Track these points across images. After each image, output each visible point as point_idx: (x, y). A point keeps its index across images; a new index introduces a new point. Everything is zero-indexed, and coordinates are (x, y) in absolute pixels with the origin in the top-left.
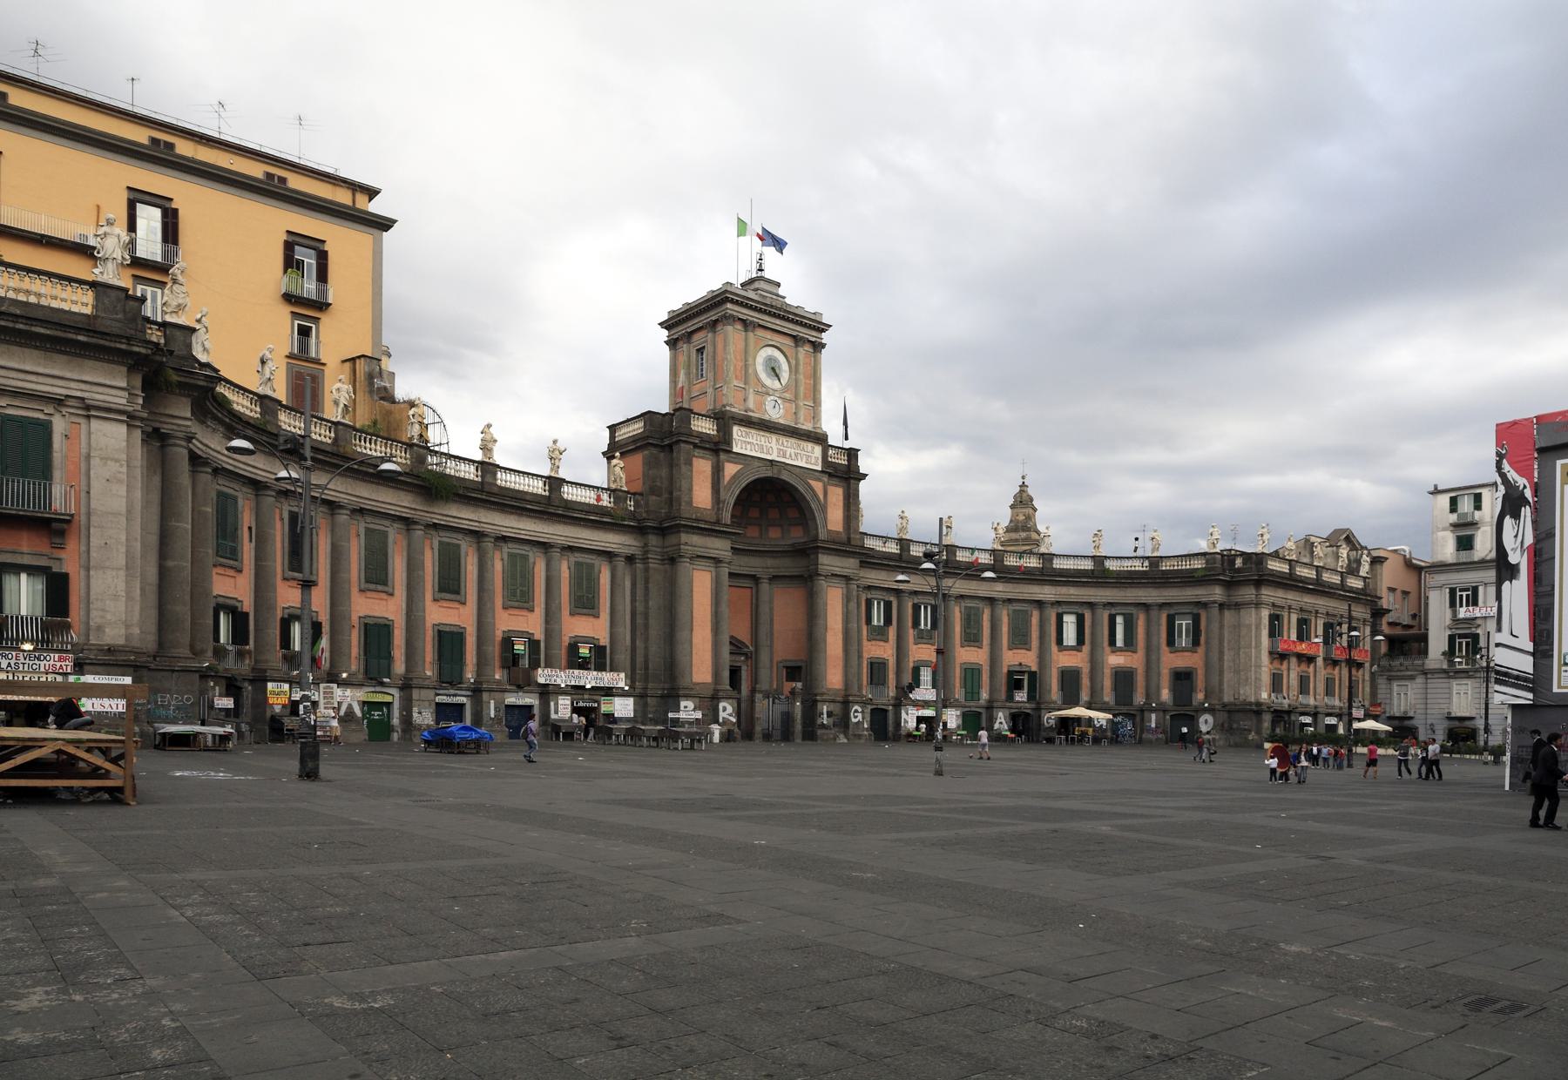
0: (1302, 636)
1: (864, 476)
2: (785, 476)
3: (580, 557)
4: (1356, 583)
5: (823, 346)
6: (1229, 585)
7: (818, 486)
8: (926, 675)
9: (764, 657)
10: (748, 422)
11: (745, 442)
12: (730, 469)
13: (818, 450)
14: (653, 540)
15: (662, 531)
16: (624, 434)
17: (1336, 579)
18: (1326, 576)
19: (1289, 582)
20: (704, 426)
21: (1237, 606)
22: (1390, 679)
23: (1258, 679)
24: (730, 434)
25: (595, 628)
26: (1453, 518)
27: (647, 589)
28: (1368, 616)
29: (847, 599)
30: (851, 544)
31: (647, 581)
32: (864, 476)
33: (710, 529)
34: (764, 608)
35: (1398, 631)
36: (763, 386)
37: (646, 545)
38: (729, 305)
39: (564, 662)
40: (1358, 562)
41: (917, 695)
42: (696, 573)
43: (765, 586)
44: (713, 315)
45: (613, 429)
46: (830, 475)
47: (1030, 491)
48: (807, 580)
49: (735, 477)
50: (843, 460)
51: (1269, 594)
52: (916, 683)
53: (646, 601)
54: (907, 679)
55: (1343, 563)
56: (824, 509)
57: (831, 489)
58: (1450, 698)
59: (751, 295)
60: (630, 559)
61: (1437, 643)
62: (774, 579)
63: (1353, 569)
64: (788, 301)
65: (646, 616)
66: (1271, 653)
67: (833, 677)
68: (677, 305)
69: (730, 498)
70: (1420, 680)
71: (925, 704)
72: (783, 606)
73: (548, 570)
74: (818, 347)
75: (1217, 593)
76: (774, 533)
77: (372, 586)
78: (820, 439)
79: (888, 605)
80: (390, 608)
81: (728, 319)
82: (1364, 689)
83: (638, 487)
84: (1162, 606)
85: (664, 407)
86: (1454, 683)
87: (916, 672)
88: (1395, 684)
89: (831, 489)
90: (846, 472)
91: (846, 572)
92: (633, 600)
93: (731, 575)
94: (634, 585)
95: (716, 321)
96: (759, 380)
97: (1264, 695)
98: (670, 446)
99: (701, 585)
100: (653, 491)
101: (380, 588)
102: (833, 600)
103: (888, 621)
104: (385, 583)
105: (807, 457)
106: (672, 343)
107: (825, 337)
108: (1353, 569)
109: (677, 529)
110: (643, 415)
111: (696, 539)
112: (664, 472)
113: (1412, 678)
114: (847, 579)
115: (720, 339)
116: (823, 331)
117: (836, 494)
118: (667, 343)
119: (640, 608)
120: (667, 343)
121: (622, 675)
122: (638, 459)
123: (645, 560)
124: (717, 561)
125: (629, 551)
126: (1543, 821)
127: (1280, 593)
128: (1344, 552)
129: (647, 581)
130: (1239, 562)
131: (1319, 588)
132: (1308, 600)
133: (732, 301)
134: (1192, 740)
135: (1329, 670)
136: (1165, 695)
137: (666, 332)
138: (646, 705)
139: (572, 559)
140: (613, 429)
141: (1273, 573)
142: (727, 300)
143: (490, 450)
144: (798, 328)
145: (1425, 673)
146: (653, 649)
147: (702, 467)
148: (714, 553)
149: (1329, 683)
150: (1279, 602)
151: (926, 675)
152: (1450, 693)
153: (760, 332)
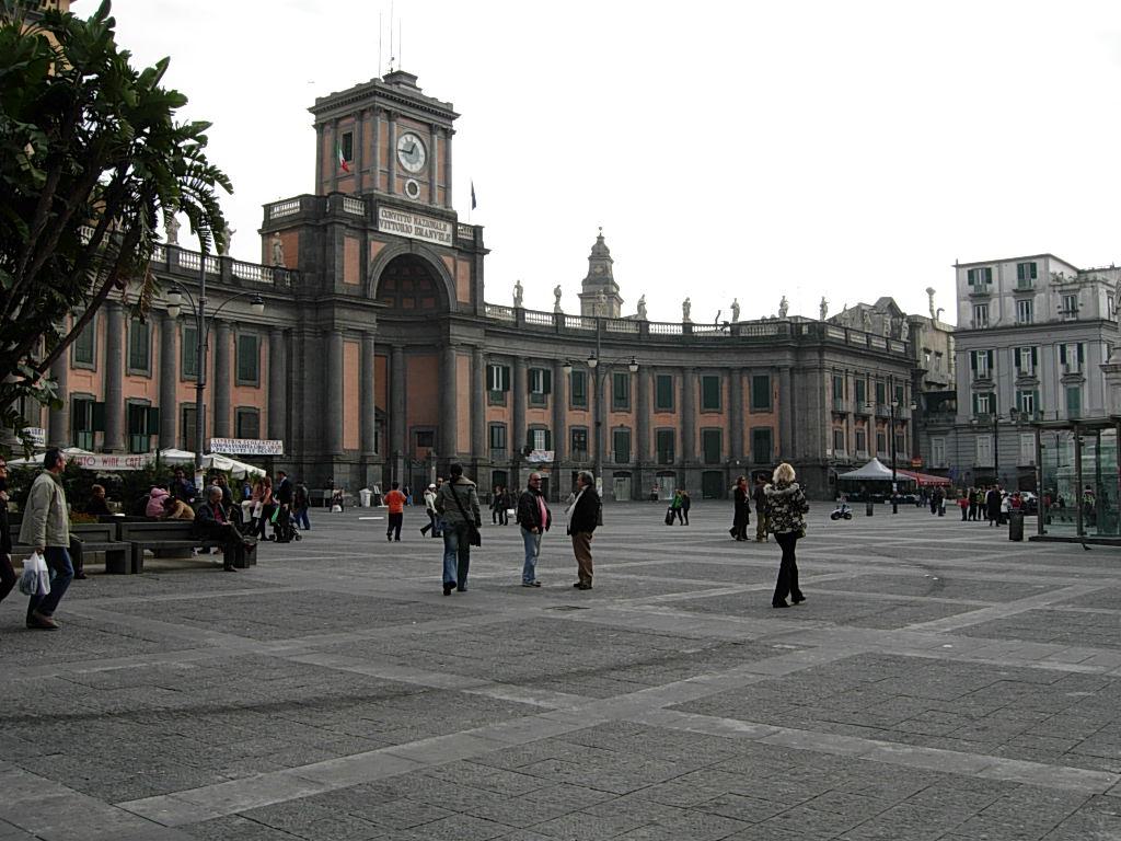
0: (859, 397)
1: (488, 251)
2: (422, 253)
3: (244, 331)
4: (898, 348)
5: (454, 132)
6: (797, 351)
7: (448, 261)
8: (539, 438)
9: (399, 422)
10: (393, 204)
11: (391, 223)
12: (376, 248)
13: (449, 227)
14: (308, 313)
15: (316, 306)
16: (276, 213)
17: (883, 345)
18: (875, 342)
19: (845, 348)
20: (353, 208)
21: (806, 370)
22: (929, 434)
23: (823, 438)
24: (377, 214)
25: (243, 397)
26: (971, 289)
27: (302, 361)
28: (909, 378)
29: (474, 367)
30: (475, 311)
31: (301, 353)
32: (488, 251)
33: (358, 303)
34: (398, 376)
35: (933, 389)
36: (405, 170)
37: (302, 319)
38: (377, 98)
39: (232, 432)
40: (900, 328)
41: (532, 458)
42: (346, 345)
43: (399, 355)
44: (360, 106)
45: (268, 208)
46: (460, 250)
47: (606, 242)
48: (439, 350)
49: (380, 255)
50: (467, 236)
51: (831, 360)
52: (530, 449)
53: (301, 372)
54: (524, 442)
55: (887, 330)
56: (454, 283)
57: (459, 263)
58: (975, 451)
59: (395, 88)
60: (287, 332)
61: (965, 410)
62: (407, 348)
63: (895, 337)
64: (424, 93)
65: (301, 387)
66: (832, 412)
67: (462, 444)
68: (325, 94)
69: (376, 276)
70: (952, 434)
71: (541, 466)
72: (414, 372)
73: (217, 344)
74: (448, 133)
75: (788, 359)
76: (408, 304)
77: (80, 364)
78: (451, 218)
79: (506, 370)
80: (613, 420)
81: (375, 110)
82: (908, 443)
83: (294, 264)
84: (743, 370)
85: (312, 192)
86: (978, 436)
87: (531, 434)
88: (933, 439)
89: (459, 263)
90: (472, 247)
91: (473, 341)
92: (289, 371)
93: (375, 344)
94: (289, 356)
95: (363, 112)
96: (400, 164)
97: (829, 452)
98: (325, 226)
99: (349, 356)
100: (309, 268)
101: (86, 365)
102: (461, 368)
103: (506, 387)
104: (145, 368)
105: (436, 235)
106: (319, 127)
107: (456, 124)
108: (895, 337)
109: (332, 304)
110: (300, 197)
111: (346, 313)
112: (319, 251)
113: (945, 433)
114: (474, 348)
115: (367, 125)
116: (454, 119)
117: (464, 268)
118: (315, 126)
119: (295, 378)
120: (315, 126)
121: (280, 443)
122: (295, 235)
123: (301, 333)
124: (364, 334)
125: (289, 325)
126: (231, 193)
127: (839, 358)
128: (888, 319)
129: (301, 353)
130: (805, 330)
131: (867, 353)
132: (861, 364)
133: (380, 95)
134: (784, 605)
135: (859, 426)
136: (749, 455)
137: (313, 117)
138: (301, 471)
139: (238, 334)
140: (268, 208)
141: (833, 341)
142: (375, 93)
143: (175, 234)
144: (433, 117)
145: (955, 428)
146: (307, 418)
147: (351, 246)
148: (362, 326)
149: (880, 438)
150: (838, 366)
151: (539, 438)
152: (1019, 445)
153: (400, 120)
